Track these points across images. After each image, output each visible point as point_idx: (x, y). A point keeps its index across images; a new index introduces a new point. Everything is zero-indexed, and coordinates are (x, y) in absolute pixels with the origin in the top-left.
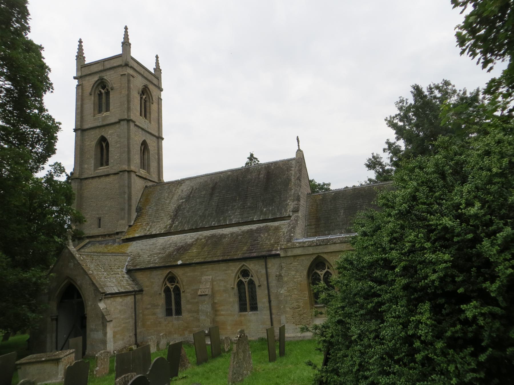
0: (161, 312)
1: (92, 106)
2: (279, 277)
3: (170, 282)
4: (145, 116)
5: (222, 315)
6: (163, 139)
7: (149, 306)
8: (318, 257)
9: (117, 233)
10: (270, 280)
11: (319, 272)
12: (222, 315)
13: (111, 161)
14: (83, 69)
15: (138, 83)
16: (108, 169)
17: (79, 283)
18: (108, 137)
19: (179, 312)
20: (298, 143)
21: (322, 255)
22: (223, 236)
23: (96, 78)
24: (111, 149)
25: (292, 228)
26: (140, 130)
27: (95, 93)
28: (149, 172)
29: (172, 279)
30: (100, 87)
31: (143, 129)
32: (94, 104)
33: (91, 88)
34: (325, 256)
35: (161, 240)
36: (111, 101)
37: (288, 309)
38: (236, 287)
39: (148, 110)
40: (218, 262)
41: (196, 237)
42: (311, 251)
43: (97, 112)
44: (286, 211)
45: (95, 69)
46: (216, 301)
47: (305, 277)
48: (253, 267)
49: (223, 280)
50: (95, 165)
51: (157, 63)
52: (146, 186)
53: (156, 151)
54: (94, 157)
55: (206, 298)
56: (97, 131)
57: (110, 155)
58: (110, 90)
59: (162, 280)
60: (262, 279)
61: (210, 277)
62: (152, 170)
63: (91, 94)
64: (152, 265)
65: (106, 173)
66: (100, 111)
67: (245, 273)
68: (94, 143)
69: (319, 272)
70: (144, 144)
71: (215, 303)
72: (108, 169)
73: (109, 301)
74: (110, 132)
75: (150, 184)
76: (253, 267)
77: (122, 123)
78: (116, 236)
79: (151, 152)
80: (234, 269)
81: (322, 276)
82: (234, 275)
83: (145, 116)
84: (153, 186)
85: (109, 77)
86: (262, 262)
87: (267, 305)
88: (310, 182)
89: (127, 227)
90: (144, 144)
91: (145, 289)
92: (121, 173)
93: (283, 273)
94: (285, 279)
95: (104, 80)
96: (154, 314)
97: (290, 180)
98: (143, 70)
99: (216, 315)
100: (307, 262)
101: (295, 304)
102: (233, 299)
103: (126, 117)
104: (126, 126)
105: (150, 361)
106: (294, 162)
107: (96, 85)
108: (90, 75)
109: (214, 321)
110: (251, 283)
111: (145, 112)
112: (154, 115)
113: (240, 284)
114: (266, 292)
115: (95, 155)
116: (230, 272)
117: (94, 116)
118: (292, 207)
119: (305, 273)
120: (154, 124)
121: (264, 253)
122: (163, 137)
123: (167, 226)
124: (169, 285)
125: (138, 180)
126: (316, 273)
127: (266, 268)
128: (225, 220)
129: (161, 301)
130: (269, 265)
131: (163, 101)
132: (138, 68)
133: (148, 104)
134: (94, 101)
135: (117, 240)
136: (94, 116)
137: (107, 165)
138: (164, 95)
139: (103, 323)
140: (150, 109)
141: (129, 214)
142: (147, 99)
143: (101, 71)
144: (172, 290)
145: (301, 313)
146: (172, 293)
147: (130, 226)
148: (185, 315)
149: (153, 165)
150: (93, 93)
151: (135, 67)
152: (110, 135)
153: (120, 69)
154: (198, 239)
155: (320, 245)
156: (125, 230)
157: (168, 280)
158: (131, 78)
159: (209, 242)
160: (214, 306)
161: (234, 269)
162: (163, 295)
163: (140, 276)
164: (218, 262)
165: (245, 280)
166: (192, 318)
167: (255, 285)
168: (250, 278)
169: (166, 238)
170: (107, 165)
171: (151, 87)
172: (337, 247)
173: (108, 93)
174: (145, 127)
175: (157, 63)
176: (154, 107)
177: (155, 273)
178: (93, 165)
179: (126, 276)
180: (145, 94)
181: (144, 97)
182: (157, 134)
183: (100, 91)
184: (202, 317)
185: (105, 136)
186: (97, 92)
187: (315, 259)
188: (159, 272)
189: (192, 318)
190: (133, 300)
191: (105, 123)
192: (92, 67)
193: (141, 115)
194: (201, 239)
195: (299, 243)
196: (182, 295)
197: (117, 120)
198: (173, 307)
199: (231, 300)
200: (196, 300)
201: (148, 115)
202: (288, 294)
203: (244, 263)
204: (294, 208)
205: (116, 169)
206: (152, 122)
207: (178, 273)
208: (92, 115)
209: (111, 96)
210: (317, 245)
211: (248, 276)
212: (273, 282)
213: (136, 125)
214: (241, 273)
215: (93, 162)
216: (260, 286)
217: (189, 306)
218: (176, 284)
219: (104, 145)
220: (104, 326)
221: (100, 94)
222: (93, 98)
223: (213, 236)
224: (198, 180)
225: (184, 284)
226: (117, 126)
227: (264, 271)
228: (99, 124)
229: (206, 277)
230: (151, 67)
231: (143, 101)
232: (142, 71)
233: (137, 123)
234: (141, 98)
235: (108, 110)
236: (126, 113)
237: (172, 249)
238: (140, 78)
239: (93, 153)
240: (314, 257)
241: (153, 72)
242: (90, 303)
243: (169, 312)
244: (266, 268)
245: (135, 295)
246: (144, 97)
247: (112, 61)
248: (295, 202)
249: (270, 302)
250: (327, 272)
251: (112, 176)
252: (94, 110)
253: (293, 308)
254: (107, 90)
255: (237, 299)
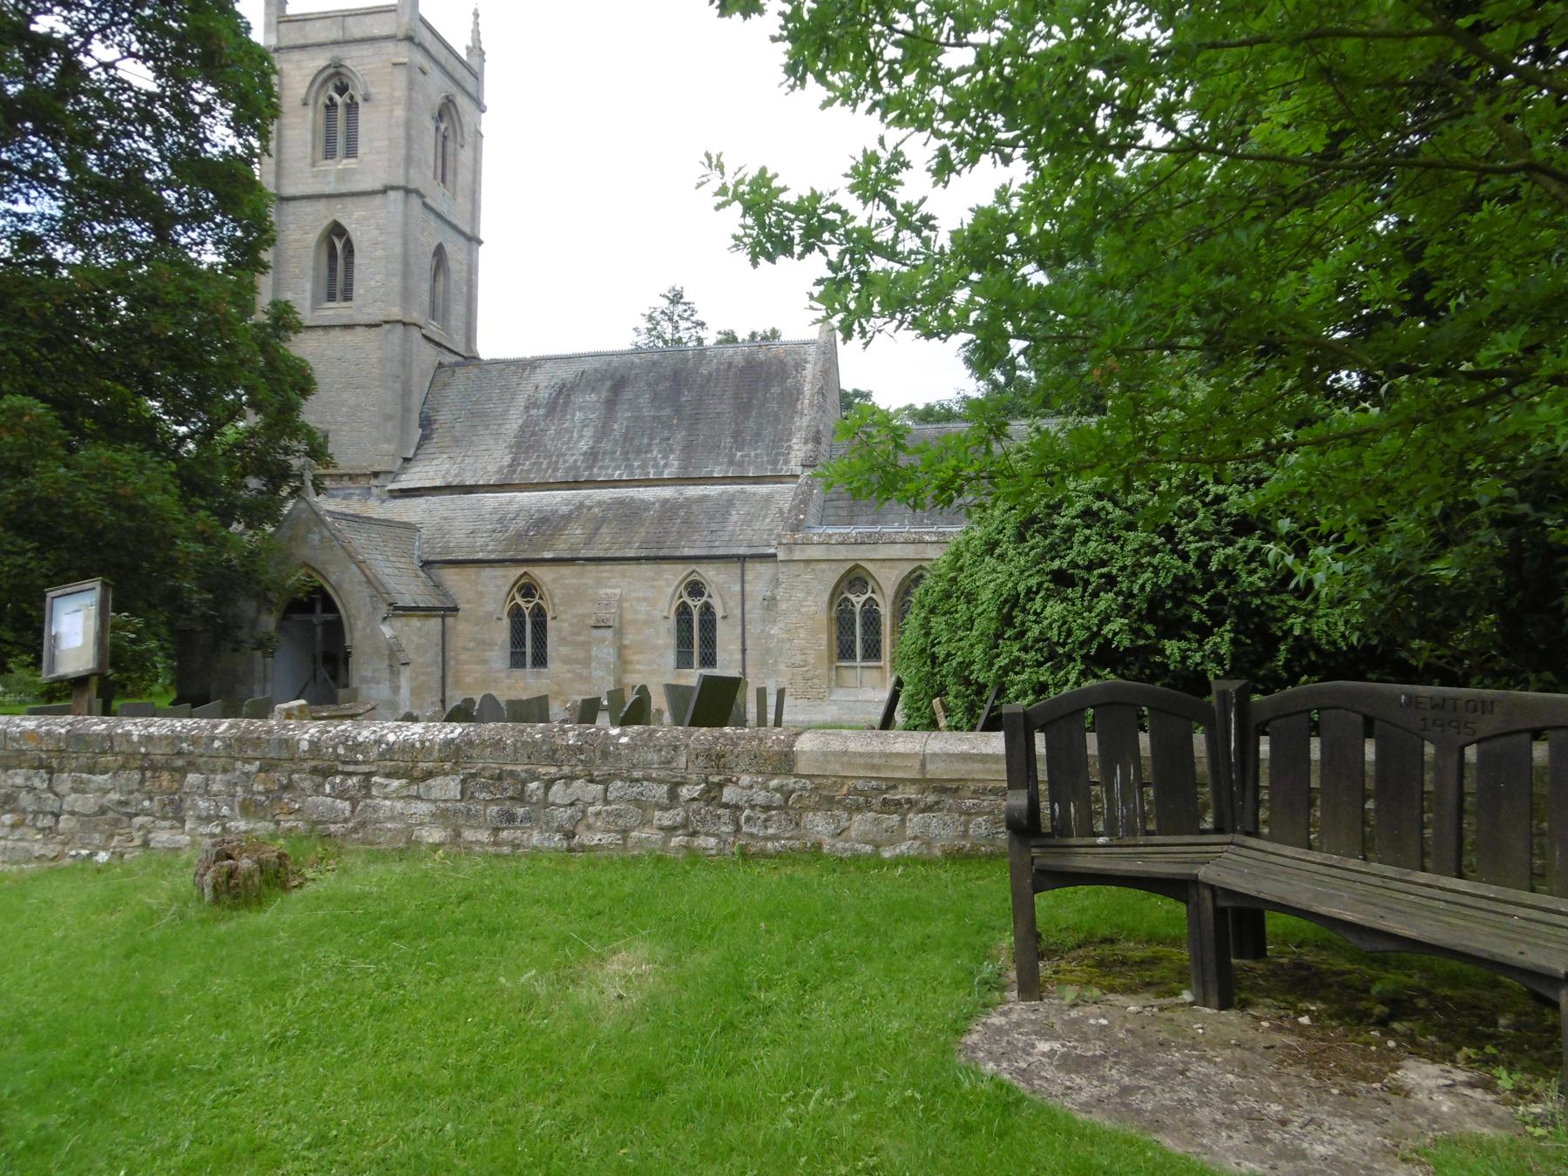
0: (499, 656)
1: (309, 136)
2: (771, 602)
3: (524, 596)
4: (443, 180)
5: (639, 672)
6: (480, 242)
7: (472, 645)
8: (856, 567)
9: (376, 475)
10: (747, 607)
11: (852, 597)
12: (639, 672)
13: (358, 290)
14: (282, 26)
15: (435, 87)
16: (349, 312)
17: (333, 578)
18: (351, 227)
19: (540, 660)
20: (476, 24)
21: (863, 564)
22: (646, 505)
23: (320, 60)
24: (358, 260)
25: (802, 502)
26: (432, 217)
27: (316, 102)
28: (445, 327)
29: (528, 589)
30: (331, 86)
31: (439, 215)
32: (314, 132)
33: (307, 84)
34: (869, 566)
35: (491, 500)
36: (361, 130)
37: (782, 667)
38: (673, 617)
39: (449, 163)
40: (637, 559)
41: (576, 501)
42: (842, 553)
43: (320, 154)
44: (786, 462)
45: (317, 33)
46: (626, 642)
47: (825, 605)
48: (711, 575)
49: (644, 599)
50: (314, 296)
51: (476, 33)
52: (440, 365)
53: (465, 275)
54: (311, 273)
55: (609, 633)
56: (321, 206)
57: (356, 275)
58: (359, 99)
59: (507, 589)
60: (731, 604)
61: (618, 591)
62: (453, 323)
63: (305, 104)
64: (480, 556)
65: (345, 321)
66: (330, 153)
67: (696, 589)
68: (312, 237)
69: (852, 597)
70: (439, 252)
71: (625, 647)
72: (349, 312)
73: (398, 623)
74: (358, 214)
75: (449, 359)
76: (711, 575)
77: (392, 194)
78: (374, 482)
79: (454, 276)
80: (674, 576)
81: (858, 607)
82: (671, 590)
83: (443, 180)
84: (457, 364)
85: (360, 62)
86: (735, 568)
87: (739, 656)
88: (848, 400)
89: (399, 462)
90: (439, 252)
91: (460, 606)
92: (387, 327)
93: (780, 593)
94: (783, 606)
95: (342, 70)
96: (484, 662)
97: (800, 392)
98: (445, 52)
99: (625, 671)
100: (833, 575)
101: (798, 659)
102: (665, 637)
103: (401, 182)
104: (400, 207)
105: (624, 704)
106: (812, 349)
107: (320, 80)
108: (303, 47)
109: (619, 680)
110: (707, 609)
111: (444, 173)
112: (464, 177)
113: (683, 613)
114: (739, 631)
115: (315, 269)
116: (662, 583)
117: (313, 165)
118: (801, 454)
119: (826, 597)
120: (463, 202)
121: (741, 551)
122: (482, 237)
123: (501, 468)
124: (519, 600)
125: (429, 349)
126: (846, 599)
127: (743, 582)
128: (643, 467)
129: (502, 632)
130: (749, 576)
131: (485, 141)
132: (435, 48)
133: (450, 145)
134: (314, 122)
135: (374, 490)
136: (313, 165)
137: (348, 298)
138: (487, 123)
139: (391, 666)
140: (456, 161)
141: (404, 430)
142: (450, 134)
143: (336, 43)
144: (527, 612)
145: (809, 675)
146: (528, 619)
147: (407, 460)
148: (554, 666)
149: (458, 309)
150: (311, 101)
151: (427, 45)
152: (356, 220)
153: (390, 47)
154: (581, 505)
155: (863, 543)
156: (395, 468)
157: (519, 591)
158: (420, 76)
159: (610, 514)
160: (621, 649)
161: (674, 576)
162: (506, 622)
163: (450, 577)
164: (637, 559)
165: (527, 607)
166: (570, 675)
167: (714, 614)
168: (704, 599)
169: (504, 496)
170: (348, 298)
171: (462, 101)
172: (897, 551)
173: (352, 107)
174: (443, 208)
175: (476, 33)
176: (465, 155)
177: (488, 572)
178: (308, 295)
179: (421, 573)
180: (446, 119)
181: (443, 126)
182: (467, 229)
183: (331, 99)
184: (597, 673)
185: (344, 222)
186: (323, 100)
187: (850, 571)
188: (498, 572)
189: (570, 675)
190: (439, 627)
191: (344, 189)
192: (309, 26)
193: (435, 177)
194: (590, 508)
195: (820, 535)
196: (550, 624)
197: (378, 186)
198: (529, 649)
199: (661, 642)
200: (582, 638)
201: (449, 177)
202: (785, 636)
203: (693, 567)
204: (807, 458)
205: (375, 313)
206: (460, 199)
207: (542, 574)
208: (309, 160)
209: (361, 117)
210: (856, 543)
211: (702, 594)
212: (755, 612)
213: (425, 205)
214: (686, 588)
215: (308, 286)
216: (724, 617)
217: (564, 650)
218: (536, 600)
219: (339, 245)
220: (394, 673)
221: (331, 106)
222: (310, 114)
223: (620, 502)
224: (588, 366)
225: (556, 600)
226: (378, 200)
227: (737, 588)
228: (327, 190)
229: (610, 591)
230: (460, 44)
231: (440, 139)
232: (441, 54)
233: (428, 201)
234: (437, 129)
235: (351, 152)
236: (401, 171)
237: (521, 524)
238: (435, 74)
239: (308, 263)
240: (849, 565)
241: (463, 54)
242: (360, 624)
243: (517, 660)
244: (743, 582)
245: (443, 617)
246: (443, 126)
247: (368, 20)
248: (810, 446)
249: (744, 651)
250: (870, 599)
251: (359, 329)
252: (314, 147)
253: (793, 665)
254: (352, 97)
255: (673, 641)
